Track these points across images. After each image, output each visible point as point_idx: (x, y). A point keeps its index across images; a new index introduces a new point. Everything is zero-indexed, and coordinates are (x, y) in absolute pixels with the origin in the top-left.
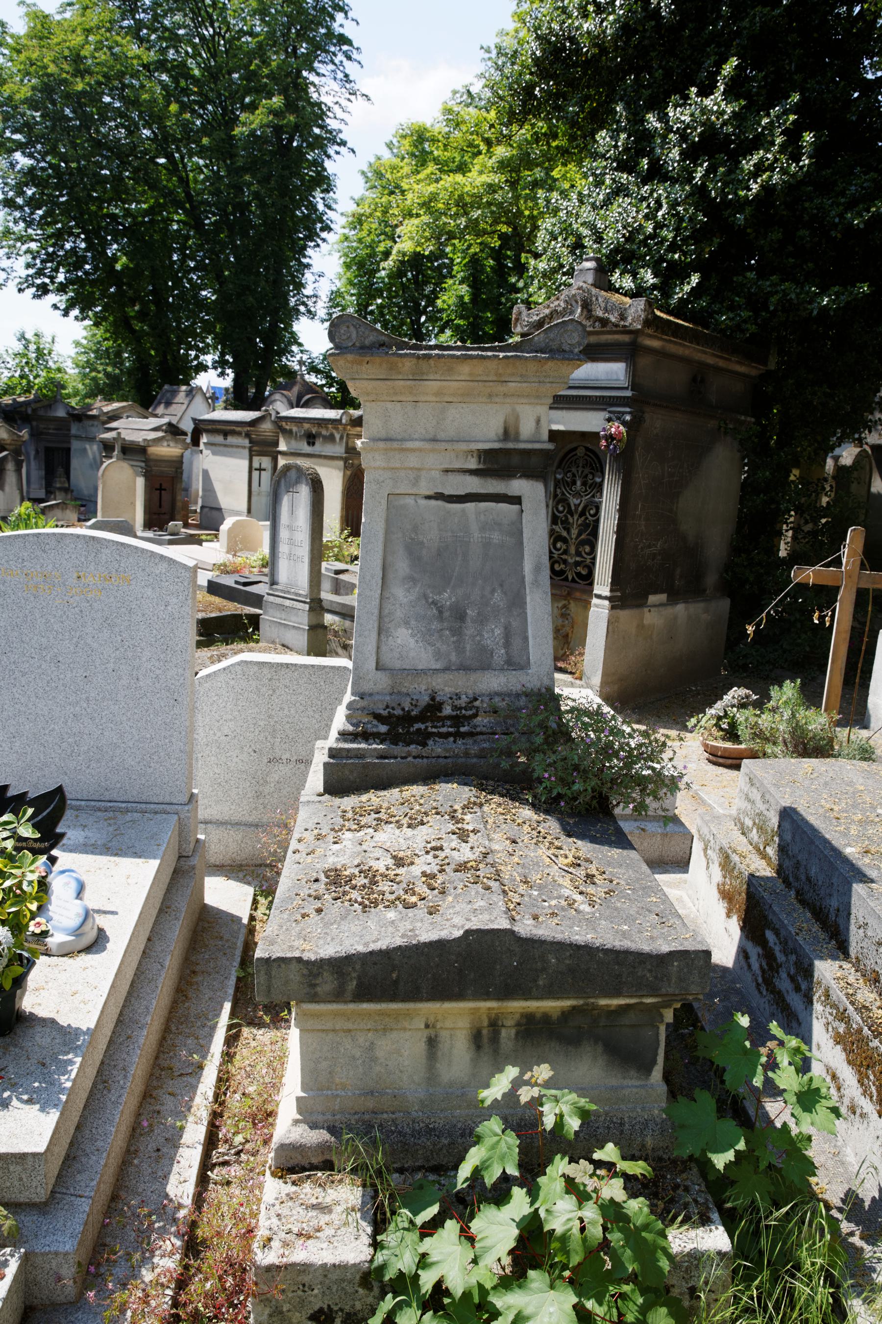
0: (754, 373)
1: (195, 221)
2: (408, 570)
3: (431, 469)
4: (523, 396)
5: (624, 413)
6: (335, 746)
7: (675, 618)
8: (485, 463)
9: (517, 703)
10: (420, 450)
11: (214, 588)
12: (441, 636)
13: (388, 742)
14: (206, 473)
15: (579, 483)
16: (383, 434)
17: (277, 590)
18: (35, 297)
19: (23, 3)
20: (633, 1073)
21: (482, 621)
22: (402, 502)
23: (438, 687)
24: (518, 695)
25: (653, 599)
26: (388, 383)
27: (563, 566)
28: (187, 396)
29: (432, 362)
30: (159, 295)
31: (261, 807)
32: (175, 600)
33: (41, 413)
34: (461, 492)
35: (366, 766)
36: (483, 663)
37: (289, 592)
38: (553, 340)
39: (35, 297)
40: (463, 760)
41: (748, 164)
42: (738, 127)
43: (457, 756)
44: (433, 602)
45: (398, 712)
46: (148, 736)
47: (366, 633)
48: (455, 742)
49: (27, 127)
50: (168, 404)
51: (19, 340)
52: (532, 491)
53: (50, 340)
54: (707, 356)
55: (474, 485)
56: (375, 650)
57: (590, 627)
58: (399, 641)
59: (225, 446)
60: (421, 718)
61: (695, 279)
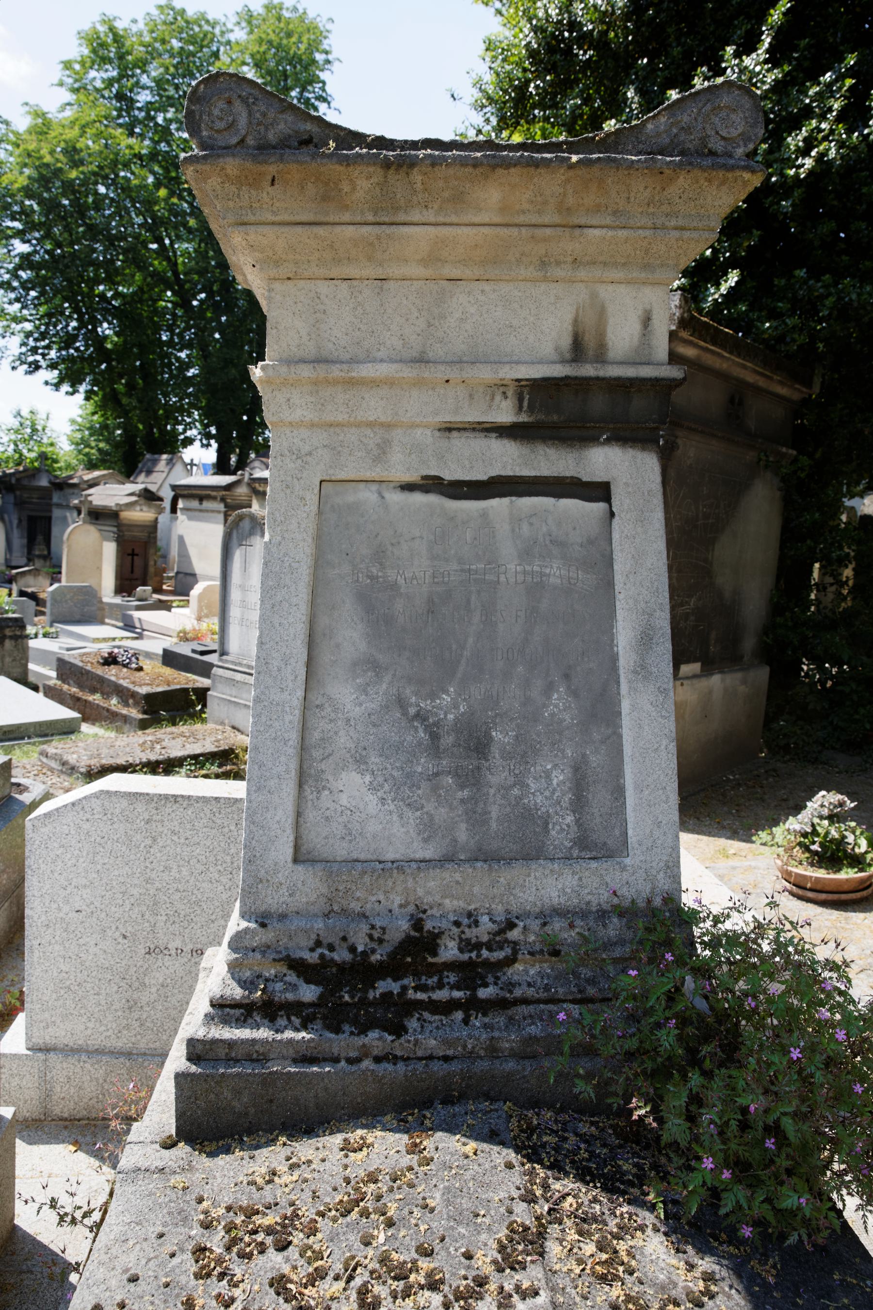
0: (796, 396)
1: (183, 300)
2: (363, 646)
3: (413, 426)
4: (615, 265)
6: (201, 1034)
7: (710, 692)
8: (531, 409)
9: (601, 932)
10: (390, 382)
11: (170, 658)
12: (435, 789)
13: (318, 1025)
14: (181, 539)
16: (310, 350)
17: (227, 661)
18: (27, 373)
19: (27, 104)
21: (524, 755)
22: (350, 498)
23: (428, 899)
24: (602, 915)
26: (320, 231)
28: (168, 464)
29: (417, 176)
30: (147, 372)
31: (136, 1024)
33: (25, 482)
34: (481, 475)
35: (269, 1080)
36: (527, 846)
37: (240, 664)
38: (687, 130)
39: (27, 373)
40: (485, 1065)
41: (795, 141)
42: (778, 103)
43: (471, 1056)
44: (417, 715)
45: (341, 955)
48: (466, 1021)
49: (25, 214)
50: (149, 472)
51: (15, 417)
52: (632, 472)
53: (45, 417)
54: (746, 371)
55: (507, 458)
56: (291, 820)
58: (344, 800)
59: (201, 511)
60: (393, 967)
61: (733, 278)
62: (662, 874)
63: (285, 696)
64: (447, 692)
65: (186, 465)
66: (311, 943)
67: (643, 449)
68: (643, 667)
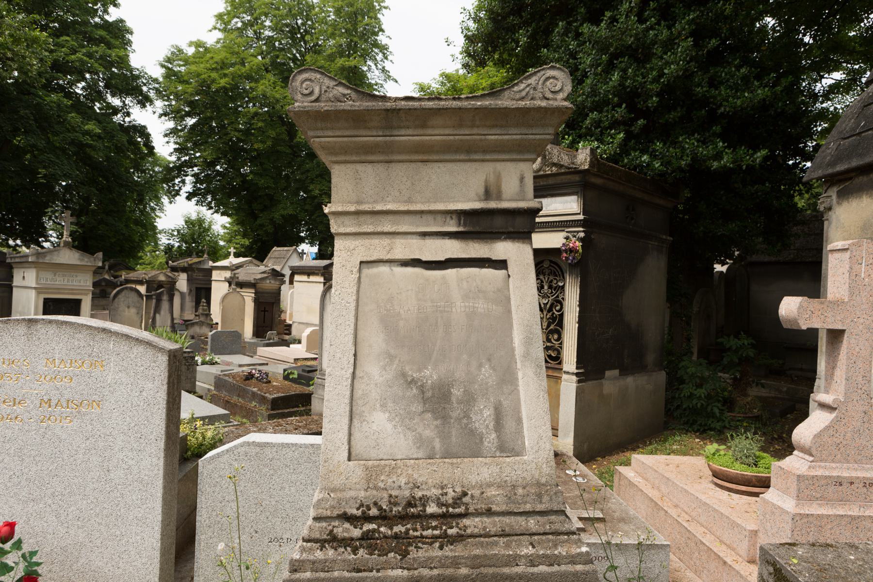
5: (578, 232)
15: (546, 287)
25: (608, 373)
32: (150, 385)
46: (118, 533)
57: (562, 397)
62: (544, 466)
63: (343, 372)
64: (427, 369)
65: (299, 253)
66: (358, 505)
67: (523, 243)
68: (528, 354)
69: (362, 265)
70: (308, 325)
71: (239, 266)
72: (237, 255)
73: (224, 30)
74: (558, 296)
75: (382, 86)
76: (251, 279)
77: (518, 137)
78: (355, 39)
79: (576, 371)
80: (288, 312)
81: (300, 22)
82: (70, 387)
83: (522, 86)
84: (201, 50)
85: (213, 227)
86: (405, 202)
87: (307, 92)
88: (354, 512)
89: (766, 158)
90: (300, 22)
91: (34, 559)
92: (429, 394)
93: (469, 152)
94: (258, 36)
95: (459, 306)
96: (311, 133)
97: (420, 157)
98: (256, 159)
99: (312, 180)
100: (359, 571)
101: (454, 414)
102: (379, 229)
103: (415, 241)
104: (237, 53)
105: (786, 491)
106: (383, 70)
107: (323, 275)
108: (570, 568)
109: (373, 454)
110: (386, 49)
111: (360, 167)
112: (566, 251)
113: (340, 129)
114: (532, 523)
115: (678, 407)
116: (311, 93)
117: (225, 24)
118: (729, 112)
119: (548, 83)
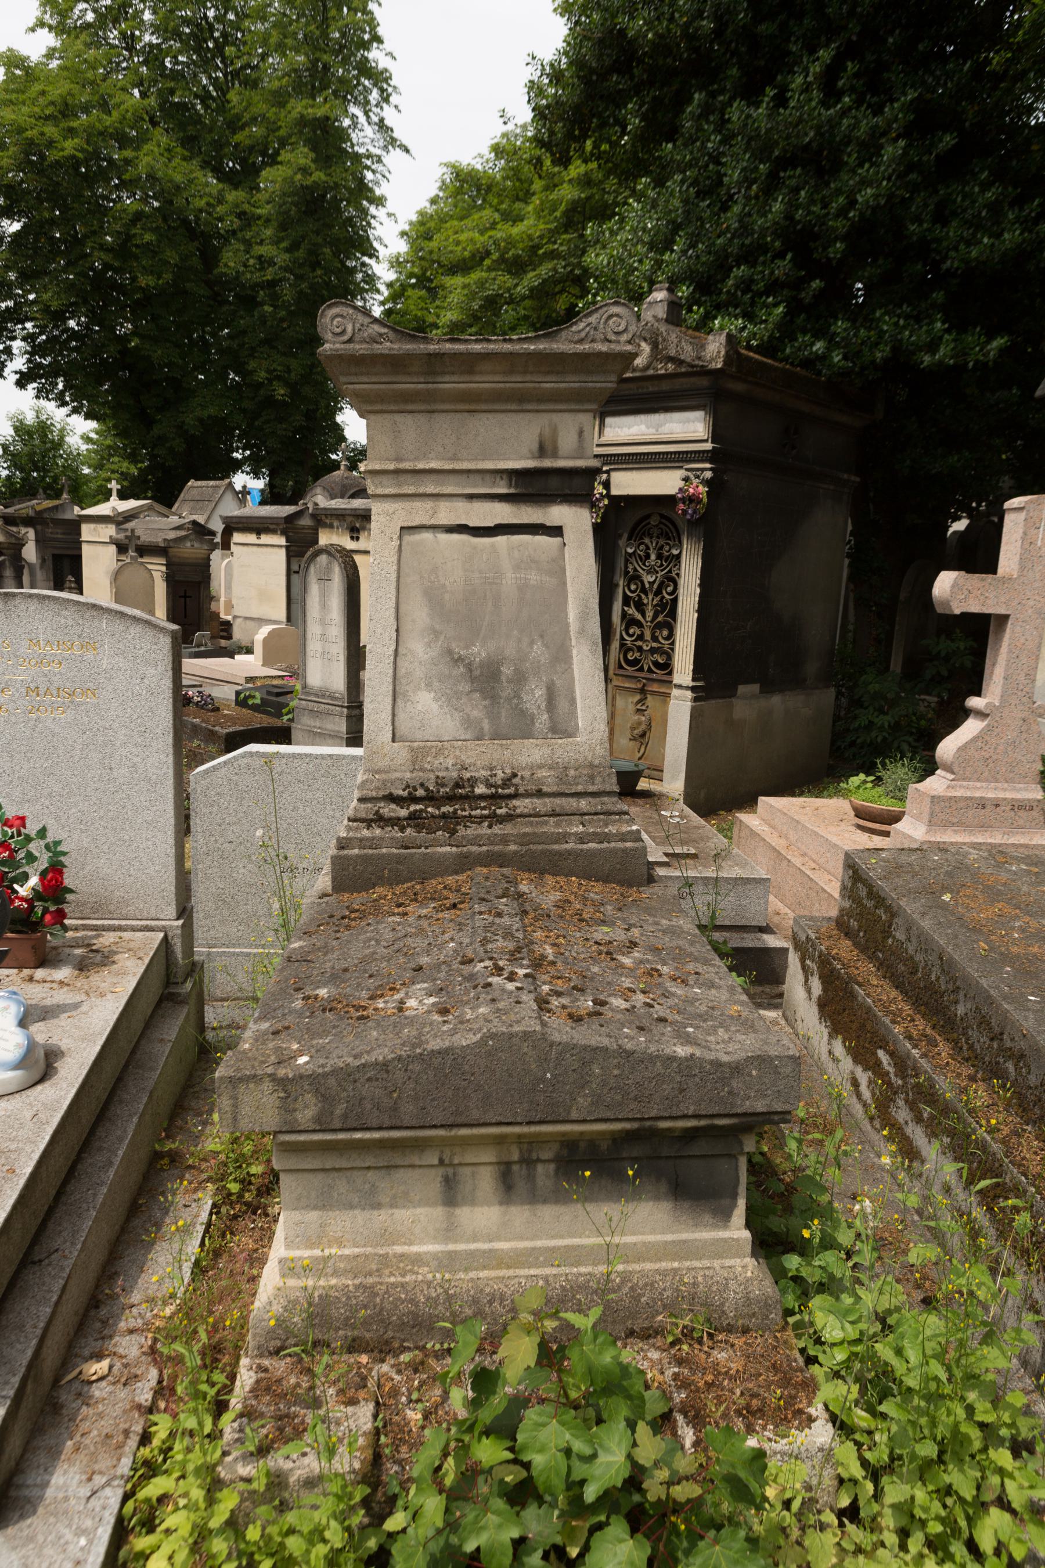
5: (703, 470)
15: (653, 557)
20: (707, 1218)
25: (742, 689)
27: (637, 654)
32: (152, 671)
34: (490, 523)
47: (380, 698)
57: (670, 722)
58: (419, 707)
65: (237, 493)
69: (405, 531)
70: (261, 621)
71: (130, 516)
72: (123, 496)
73: (59, 30)
74: (670, 571)
75: (379, 160)
76: (158, 539)
77: (576, 385)
78: (325, 57)
79: (691, 684)
80: (222, 599)
81: (211, 14)
82: (60, 673)
83: (582, 325)
84: (18, 72)
85: (67, 439)
86: (451, 459)
87: (338, 330)
88: (401, 792)
89: (1002, 351)
90: (211, 14)
91: (59, 849)
92: (477, 673)
93: (520, 401)
94: (129, 42)
95: (510, 579)
96: (343, 379)
97: (467, 407)
98: (144, 304)
99: (253, 349)
100: (407, 848)
101: (504, 694)
102: (421, 490)
103: (461, 505)
104: (93, 83)
105: (917, 818)
106: (381, 125)
107: (284, 533)
108: (620, 845)
109: (419, 735)
110: (387, 80)
111: (398, 417)
112: (683, 500)
113: (376, 374)
114: (583, 804)
115: (853, 744)
116: (344, 332)
117: (60, 14)
118: (957, 269)
119: (611, 322)
